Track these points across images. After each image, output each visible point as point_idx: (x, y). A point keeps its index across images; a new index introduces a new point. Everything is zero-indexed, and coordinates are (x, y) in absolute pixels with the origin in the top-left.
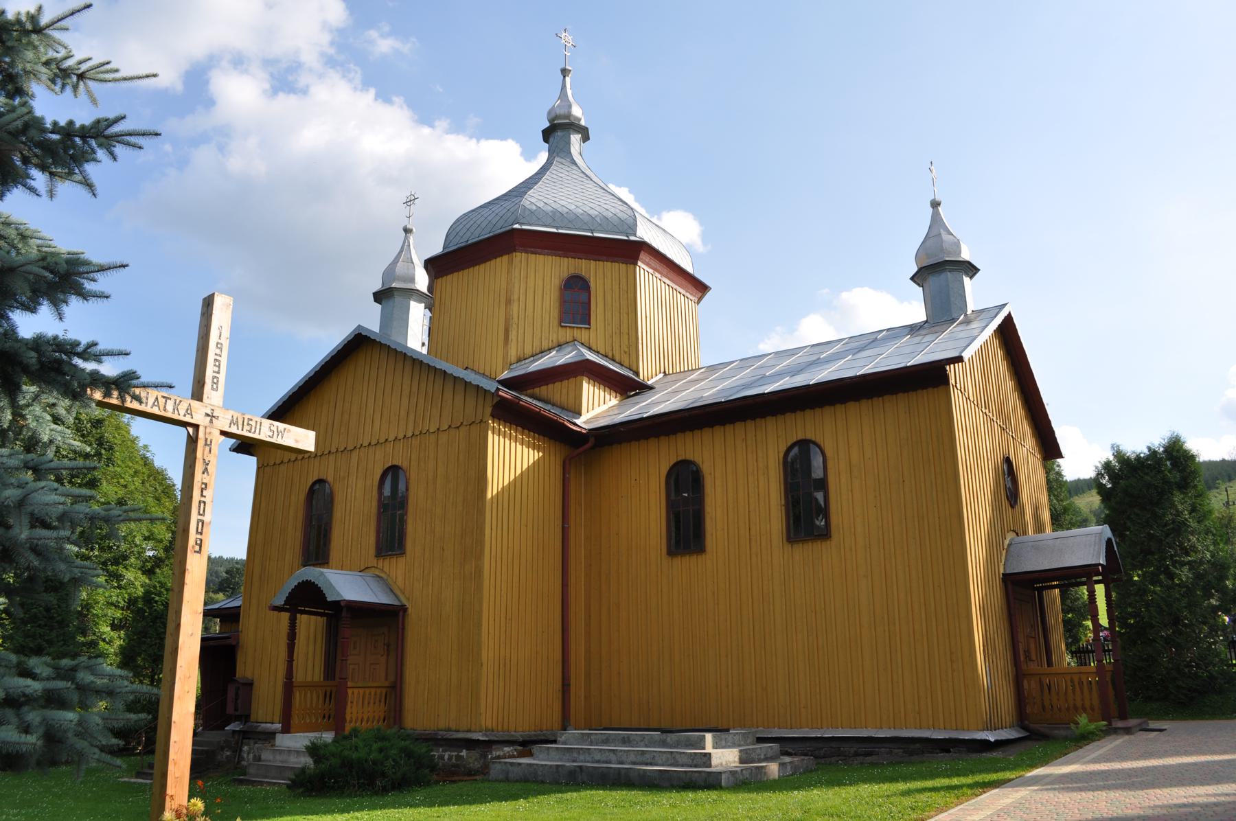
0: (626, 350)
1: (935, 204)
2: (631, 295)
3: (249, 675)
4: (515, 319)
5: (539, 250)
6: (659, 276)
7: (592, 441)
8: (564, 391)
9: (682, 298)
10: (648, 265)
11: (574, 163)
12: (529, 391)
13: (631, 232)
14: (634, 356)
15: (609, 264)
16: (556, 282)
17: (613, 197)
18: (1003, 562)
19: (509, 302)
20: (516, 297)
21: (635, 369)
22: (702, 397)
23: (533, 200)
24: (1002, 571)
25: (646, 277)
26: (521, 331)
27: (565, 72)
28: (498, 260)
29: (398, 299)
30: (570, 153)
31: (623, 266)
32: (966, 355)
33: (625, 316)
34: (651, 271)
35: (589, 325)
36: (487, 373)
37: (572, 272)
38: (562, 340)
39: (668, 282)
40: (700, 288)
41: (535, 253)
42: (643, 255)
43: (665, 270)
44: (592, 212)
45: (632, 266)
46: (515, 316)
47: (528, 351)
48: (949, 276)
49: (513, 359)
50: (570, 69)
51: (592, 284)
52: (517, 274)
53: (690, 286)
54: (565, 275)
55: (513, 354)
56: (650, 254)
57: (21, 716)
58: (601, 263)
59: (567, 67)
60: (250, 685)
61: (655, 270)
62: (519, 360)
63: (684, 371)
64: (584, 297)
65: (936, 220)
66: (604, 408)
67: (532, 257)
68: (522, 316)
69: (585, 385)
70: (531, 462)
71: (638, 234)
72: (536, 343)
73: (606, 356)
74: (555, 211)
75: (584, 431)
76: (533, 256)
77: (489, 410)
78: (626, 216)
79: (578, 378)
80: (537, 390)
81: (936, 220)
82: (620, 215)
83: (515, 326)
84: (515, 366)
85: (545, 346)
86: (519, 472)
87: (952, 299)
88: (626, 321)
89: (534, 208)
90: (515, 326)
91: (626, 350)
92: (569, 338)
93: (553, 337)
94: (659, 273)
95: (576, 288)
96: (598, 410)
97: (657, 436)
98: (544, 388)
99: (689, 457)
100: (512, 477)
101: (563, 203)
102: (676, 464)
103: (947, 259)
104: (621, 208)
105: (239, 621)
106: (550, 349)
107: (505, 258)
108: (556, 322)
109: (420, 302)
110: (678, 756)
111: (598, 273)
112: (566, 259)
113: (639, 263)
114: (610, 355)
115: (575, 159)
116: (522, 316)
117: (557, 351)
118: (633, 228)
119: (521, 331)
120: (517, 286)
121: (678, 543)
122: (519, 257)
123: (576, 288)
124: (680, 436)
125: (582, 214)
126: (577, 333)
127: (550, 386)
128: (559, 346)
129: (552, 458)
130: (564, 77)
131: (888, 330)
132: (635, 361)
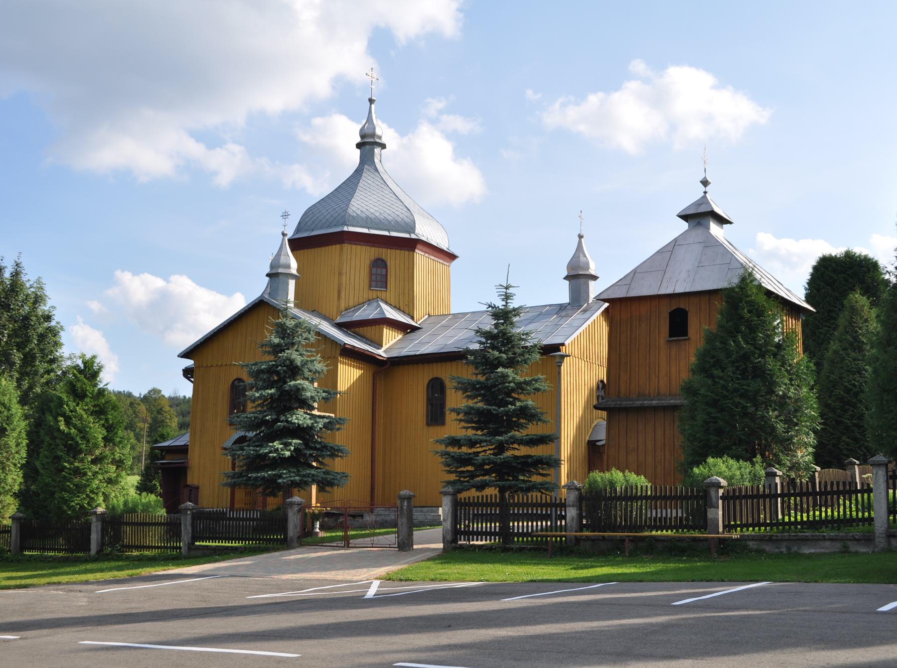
0: (407, 303)
1: (581, 237)
2: (411, 271)
3: (196, 483)
4: (344, 285)
5: (358, 243)
6: (427, 255)
7: (389, 364)
8: (373, 333)
9: (439, 264)
10: (421, 250)
11: (377, 170)
12: (352, 330)
13: (412, 231)
14: (412, 307)
15: (398, 251)
16: (368, 262)
17: (401, 204)
18: (589, 434)
19: (340, 274)
20: (344, 272)
21: (412, 315)
22: (446, 345)
23: (354, 209)
24: (587, 439)
25: (420, 258)
26: (347, 292)
27: (371, 101)
28: (334, 246)
29: (281, 277)
30: (374, 162)
31: (407, 252)
32: (566, 343)
33: (407, 283)
34: (423, 254)
35: (386, 288)
36: (327, 315)
37: (377, 256)
38: (370, 298)
39: (432, 257)
40: (452, 257)
41: (356, 244)
42: (418, 246)
43: (431, 251)
44: (389, 218)
45: (412, 252)
46: (344, 283)
47: (351, 304)
48: (582, 281)
49: (343, 309)
50: (375, 99)
51: (388, 264)
52: (345, 257)
53: (445, 257)
54: (373, 258)
55: (343, 306)
56: (424, 249)
57: (243, 487)
58: (394, 250)
59: (373, 98)
60: (197, 488)
61: (425, 252)
62: (346, 310)
63: (438, 315)
64: (384, 271)
65: (580, 247)
66: (394, 341)
67: (354, 246)
68: (348, 283)
69: (385, 330)
70: (358, 376)
71: (418, 230)
72: (356, 299)
73: (396, 307)
74: (367, 217)
75: (385, 359)
76: (355, 246)
77: (338, 352)
78: (409, 220)
79: (381, 326)
80: (357, 329)
81: (580, 247)
82: (406, 219)
83: (344, 289)
84: (344, 313)
85: (361, 301)
86: (352, 382)
87: (582, 294)
88: (407, 287)
89: (355, 215)
90: (344, 289)
91: (407, 303)
92: (375, 297)
93: (366, 296)
94: (427, 253)
95: (379, 264)
96: (391, 343)
97: (423, 363)
98: (361, 329)
99: (439, 376)
100: (349, 385)
101: (372, 211)
102: (432, 379)
103: (581, 273)
104: (406, 214)
105: (188, 453)
106: (363, 303)
107: (338, 246)
108: (367, 287)
109: (292, 279)
110: (427, 516)
111: (392, 256)
112: (373, 248)
113: (416, 251)
114: (398, 307)
115: (377, 166)
116: (348, 283)
117: (368, 304)
118: (411, 228)
119: (347, 292)
120: (345, 265)
121: (431, 420)
122: (346, 247)
123: (379, 264)
124: (435, 364)
125: (383, 219)
126: (379, 294)
127: (365, 328)
128: (369, 301)
129: (368, 372)
130: (371, 104)
131: (550, 305)
132: (412, 309)
